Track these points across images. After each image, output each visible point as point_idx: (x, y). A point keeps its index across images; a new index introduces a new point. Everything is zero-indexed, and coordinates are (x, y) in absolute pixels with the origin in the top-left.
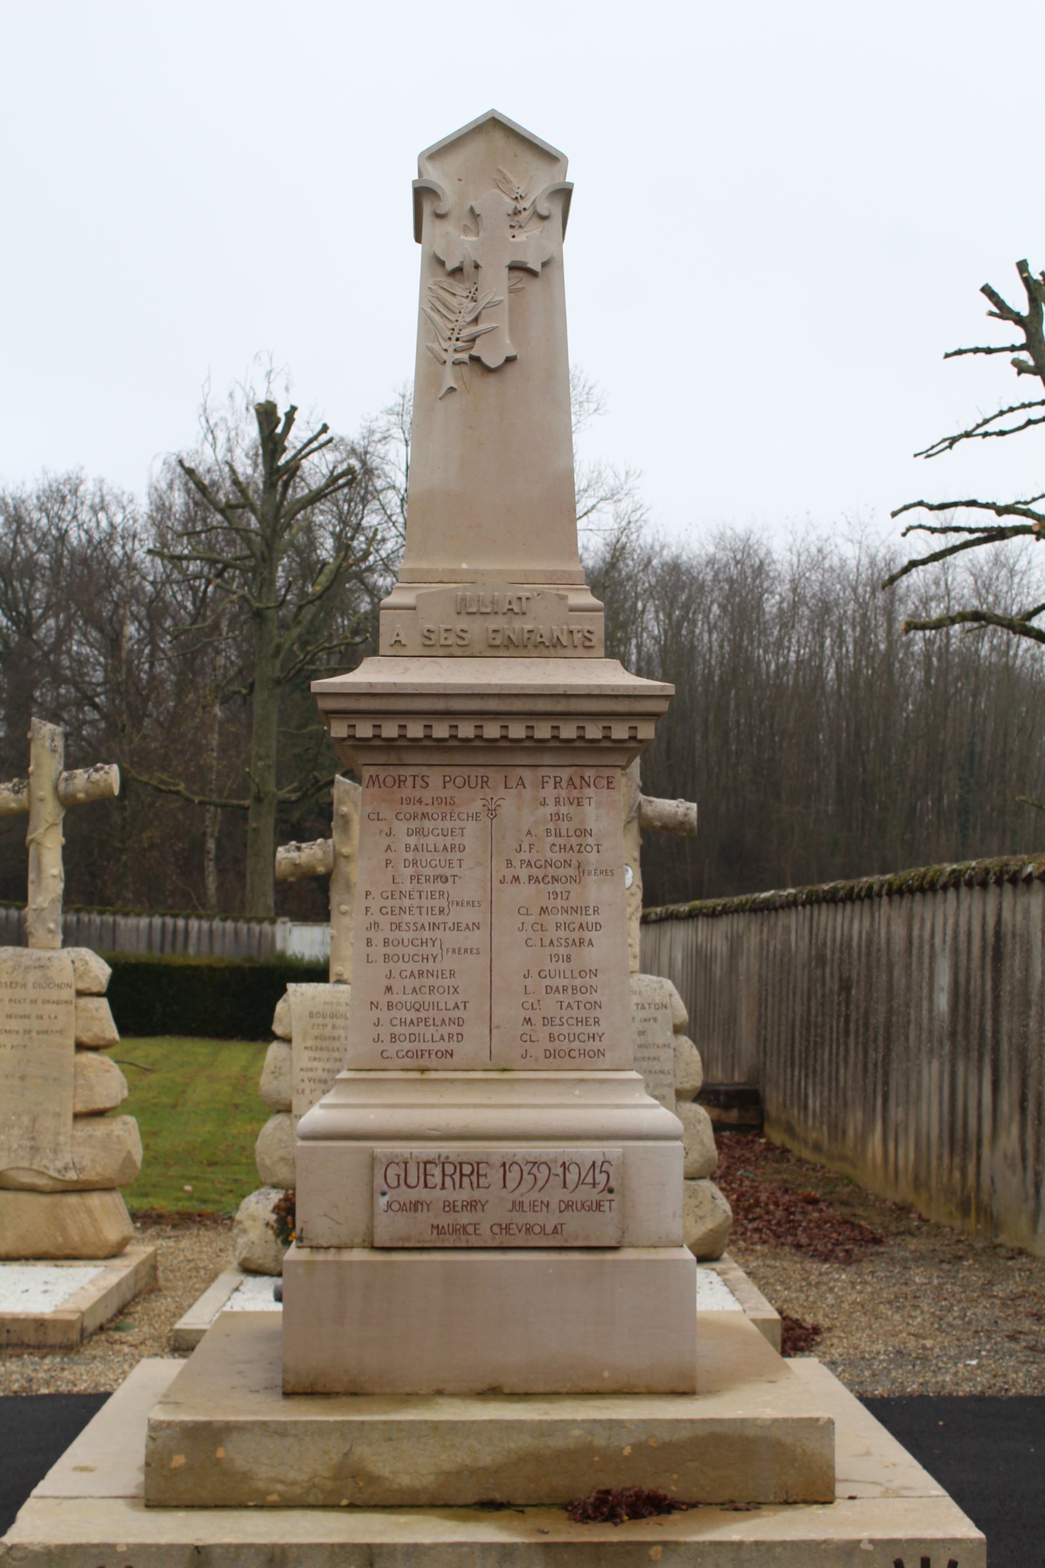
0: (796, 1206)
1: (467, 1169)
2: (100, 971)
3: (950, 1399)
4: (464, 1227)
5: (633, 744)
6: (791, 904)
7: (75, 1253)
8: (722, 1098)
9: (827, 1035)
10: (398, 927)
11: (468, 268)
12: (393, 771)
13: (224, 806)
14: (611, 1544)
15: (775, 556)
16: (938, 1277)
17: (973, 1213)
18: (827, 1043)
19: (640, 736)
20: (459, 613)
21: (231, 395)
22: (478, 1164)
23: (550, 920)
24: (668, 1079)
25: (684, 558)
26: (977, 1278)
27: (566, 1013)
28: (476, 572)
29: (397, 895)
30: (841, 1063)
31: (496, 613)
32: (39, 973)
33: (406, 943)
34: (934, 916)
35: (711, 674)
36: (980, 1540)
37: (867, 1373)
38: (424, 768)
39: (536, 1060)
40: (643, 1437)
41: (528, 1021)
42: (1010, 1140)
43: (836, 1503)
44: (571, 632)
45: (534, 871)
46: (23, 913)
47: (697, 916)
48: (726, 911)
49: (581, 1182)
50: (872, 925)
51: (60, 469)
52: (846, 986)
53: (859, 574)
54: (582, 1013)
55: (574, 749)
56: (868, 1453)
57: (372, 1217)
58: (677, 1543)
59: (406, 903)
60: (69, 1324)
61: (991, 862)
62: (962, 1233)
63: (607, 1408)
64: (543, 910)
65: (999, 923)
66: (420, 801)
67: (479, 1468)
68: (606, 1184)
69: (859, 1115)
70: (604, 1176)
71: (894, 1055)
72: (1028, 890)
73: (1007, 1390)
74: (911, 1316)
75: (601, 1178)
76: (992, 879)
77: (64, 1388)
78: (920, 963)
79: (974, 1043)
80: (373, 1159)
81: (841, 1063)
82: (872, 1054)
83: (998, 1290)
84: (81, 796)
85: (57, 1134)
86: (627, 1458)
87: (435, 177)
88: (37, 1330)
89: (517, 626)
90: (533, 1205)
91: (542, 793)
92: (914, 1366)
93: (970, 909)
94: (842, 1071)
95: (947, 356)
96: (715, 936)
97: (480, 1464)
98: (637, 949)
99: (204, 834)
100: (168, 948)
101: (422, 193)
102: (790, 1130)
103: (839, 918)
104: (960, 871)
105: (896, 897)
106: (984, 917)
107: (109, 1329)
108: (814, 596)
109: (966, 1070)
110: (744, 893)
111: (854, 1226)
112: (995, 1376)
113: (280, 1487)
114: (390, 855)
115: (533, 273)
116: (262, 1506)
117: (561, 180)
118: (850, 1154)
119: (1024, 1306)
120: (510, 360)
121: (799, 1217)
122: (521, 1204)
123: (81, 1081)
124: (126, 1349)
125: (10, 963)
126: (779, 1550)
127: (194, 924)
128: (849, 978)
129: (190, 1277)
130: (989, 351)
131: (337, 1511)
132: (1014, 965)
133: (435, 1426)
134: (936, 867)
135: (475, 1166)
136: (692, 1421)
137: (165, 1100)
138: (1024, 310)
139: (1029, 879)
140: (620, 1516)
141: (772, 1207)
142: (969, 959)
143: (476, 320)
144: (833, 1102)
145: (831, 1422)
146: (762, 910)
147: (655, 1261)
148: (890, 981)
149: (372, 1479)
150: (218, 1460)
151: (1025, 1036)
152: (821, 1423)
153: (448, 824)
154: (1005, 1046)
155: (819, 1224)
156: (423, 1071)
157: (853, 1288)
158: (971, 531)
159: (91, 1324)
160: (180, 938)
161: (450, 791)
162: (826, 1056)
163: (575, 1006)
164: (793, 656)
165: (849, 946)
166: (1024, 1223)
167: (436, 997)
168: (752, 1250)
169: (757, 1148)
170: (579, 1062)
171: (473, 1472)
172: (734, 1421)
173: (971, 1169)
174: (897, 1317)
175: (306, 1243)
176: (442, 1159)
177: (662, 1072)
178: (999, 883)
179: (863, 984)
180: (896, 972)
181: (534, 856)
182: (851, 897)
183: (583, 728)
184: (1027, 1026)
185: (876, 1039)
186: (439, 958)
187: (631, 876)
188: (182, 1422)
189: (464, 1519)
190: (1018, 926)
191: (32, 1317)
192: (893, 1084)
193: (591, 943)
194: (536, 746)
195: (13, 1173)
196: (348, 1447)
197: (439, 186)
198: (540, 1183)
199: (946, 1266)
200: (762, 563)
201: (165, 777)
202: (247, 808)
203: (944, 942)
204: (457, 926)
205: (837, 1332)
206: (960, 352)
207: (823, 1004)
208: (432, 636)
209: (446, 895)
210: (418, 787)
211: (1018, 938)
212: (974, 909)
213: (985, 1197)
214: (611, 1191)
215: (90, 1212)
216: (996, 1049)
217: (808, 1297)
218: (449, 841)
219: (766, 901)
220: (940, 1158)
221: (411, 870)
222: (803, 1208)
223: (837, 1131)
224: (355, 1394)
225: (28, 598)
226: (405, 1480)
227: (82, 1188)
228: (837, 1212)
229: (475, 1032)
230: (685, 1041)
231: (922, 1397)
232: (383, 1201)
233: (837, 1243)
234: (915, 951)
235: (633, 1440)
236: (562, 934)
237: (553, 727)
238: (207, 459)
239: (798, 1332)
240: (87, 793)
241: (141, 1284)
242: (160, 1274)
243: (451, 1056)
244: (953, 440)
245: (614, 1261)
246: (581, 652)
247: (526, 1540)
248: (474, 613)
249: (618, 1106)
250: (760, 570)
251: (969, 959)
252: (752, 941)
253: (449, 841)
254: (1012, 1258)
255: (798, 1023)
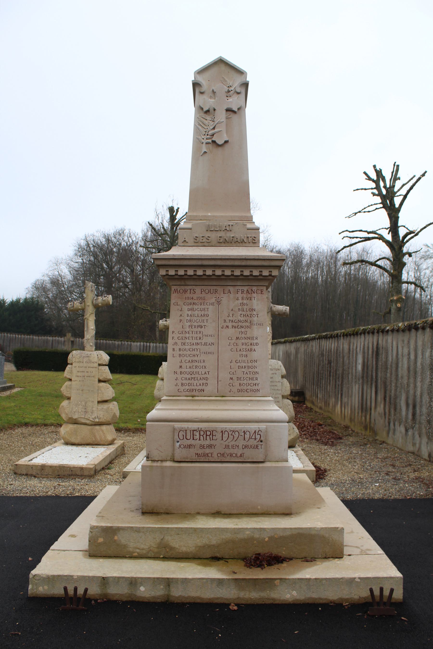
0: (315, 427)
1: (208, 433)
2: (106, 358)
3: (372, 500)
4: (207, 454)
5: (270, 278)
6: (314, 339)
7: (99, 443)
8: (293, 393)
9: (324, 376)
10: (184, 344)
11: (212, 110)
12: (183, 287)
13: (160, 313)
14: (260, 579)
15: (306, 249)
16: (360, 451)
17: (368, 429)
18: (324, 379)
19: (273, 274)
20: (207, 231)
21: (163, 206)
22: (213, 431)
23: (240, 342)
24: (280, 392)
25: (282, 249)
26: (372, 451)
27: (245, 376)
28: (214, 216)
29: (184, 332)
30: (328, 384)
31: (221, 231)
32: (87, 358)
33: (187, 350)
34: (357, 342)
35: (289, 280)
36: (401, 577)
37: (344, 489)
38: (194, 286)
39: (234, 393)
40: (273, 534)
41: (231, 379)
42: (381, 408)
43: (344, 558)
44: (248, 237)
45: (234, 324)
46: (83, 340)
47: (286, 342)
48: (295, 341)
49: (250, 438)
50: (338, 345)
51: (119, 227)
52: (330, 362)
53: (327, 254)
54: (251, 376)
55: (249, 279)
56: (352, 532)
57: (174, 450)
58: (285, 579)
59: (187, 335)
60: (90, 469)
61: (376, 326)
62: (365, 435)
63: (260, 522)
64: (237, 338)
65: (378, 344)
66: (192, 298)
67: (212, 545)
68: (259, 439)
69: (333, 399)
70: (259, 436)
71: (344, 383)
72: (387, 334)
73: (391, 496)
74: (354, 465)
75: (258, 437)
76: (376, 331)
77: (83, 494)
78: (353, 356)
79: (370, 380)
80: (174, 429)
81: (328, 384)
82: (338, 382)
83: (379, 456)
84: (100, 304)
85: (93, 407)
86: (266, 542)
87: (200, 79)
88: (81, 471)
89: (228, 235)
90: (233, 446)
91: (237, 295)
92: (358, 486)
93: (368, 340)
94: (328, 387)
95: (354, 190)
96: (291, 348)
97: (212, 544)
98: (270, 352)
99: (156, 321)
100: (145, 351)
101: (195, 85)
102: (313, 403)
103: (328, 343)
104: (365, 329)
105: (345, 337)
106: (373, 342)
107: (105, 469)
108: (316, 259)
109: (367, 388)
110: (300, 336)
111: (334, 433)
112: (385, 490)
113: (138, 550)
114: (181, 318)
115: (234, 112)
116: (132, 557)
117: (245, 80)
118: (330, 410)
119: (389, 462)
120: (226, 142)
121: (317, 430)
122: (228, 446)
123: (100, 392)
124: (109, 477)
125: (79, 356)
126: (324, 581)
127: (152, 344)
128: (331, 360)
129: (135, 450)
130: (365, 189)
131: (159, 560)
132: (382, 357)
133: (195, 530)
134: (358, 328)
135: (211, 432)
136: (291, 529)
137: (138, 393)
138: (375, 178)
139: (388, 331)
140: (263, 565)
141: (309, 427)
142: (368, 355)
143: (214, 128)
144: (326, 395)
145: (343, 529)
146: (305, 341)
147: (277, 467)
148: (343, 361)
149: (172, 548)
150: (115, 540)
151: (386, 378)
152: (339, 529)
153: (203, 307)
154: (379, 381)
155: (323, 432)
156: (193, 396)
157: (335, 455)
158: (361, 238)
159: (98, 468)
160: (148, 348)
161: (203, 295)
162: (324, 383)
163: (249, 373)
164: (310, 275)
165: (331, 351)
166: (385, 434)
167: (198, 370)
168: (304, 441)
169: (303, 408)
170: (250, 394)
171: (209, 546)
172: (306, 528)
173: (368, 417)
174: (350, 466)
175: (149, 459)
176: (199, 430)
177: (278, 390)
178: (378, 332)
179: (335, 362)
180: (345, 358)
181: (234, 319)
182: (332, 337)
183: (252, 271)
184: (386, 375)
185: (339, 378)
186: (199, 356)
187: (269, 329)
188: (102, 526)
189: (205, 565)
190: (384, 345)
191: (79, 466)
192: (344, 391)
193: (255, 350)
194: (234, 278)
195: (79, 419)
196: (163, 537)
197: (201, 82)
198: (235, 439)
199: (362, 447)
200: (302, 251)
201: (145, 306)
202: (166, 314)
203: (360, 350)
204: (206, 344)
205: (332, 471)
206: (358, 190)
207: (323, 368)
208: (197, 239)
209: (202, 333)
210: (192, 293)
211: (384, 349)
212: (370, 340)
213: (372, 425)
214: (261, 441)
215: (103, 431)
216: (376, 382)
217: (322, 458)
218: (203, 313)
219: (306, 338)
220: (358, 413)
221: (189, 324)
222: (318, 427)
223: (327, 404)
224: (168, 513)
225: (111, 260)
226: (184, 549)
227: (100, 424)
228: (328, 428)
229: (212, 382)
230: (285, 380)
231: (363, 500)
232: (178, 444)
233: (329, 439)
234: (351, 353)
235: (269, 535)
236: (244, 347)
237: (241, 271)
238: (157, 223)
239: (320, 472)
240: (102, 304)
241: (118, 453)
242: (126, 449)
243: (203, 391)
244: (356, 214)
245: (263, 467)
246: (251, 244)
247: (228, 577)
248: (212, 231)
249: (264, 410)
250: (302, 252)
251: (368, 355)
252: (302, 349)
253: (203, 313)
254: (381, 444)
255: (315, 373)
